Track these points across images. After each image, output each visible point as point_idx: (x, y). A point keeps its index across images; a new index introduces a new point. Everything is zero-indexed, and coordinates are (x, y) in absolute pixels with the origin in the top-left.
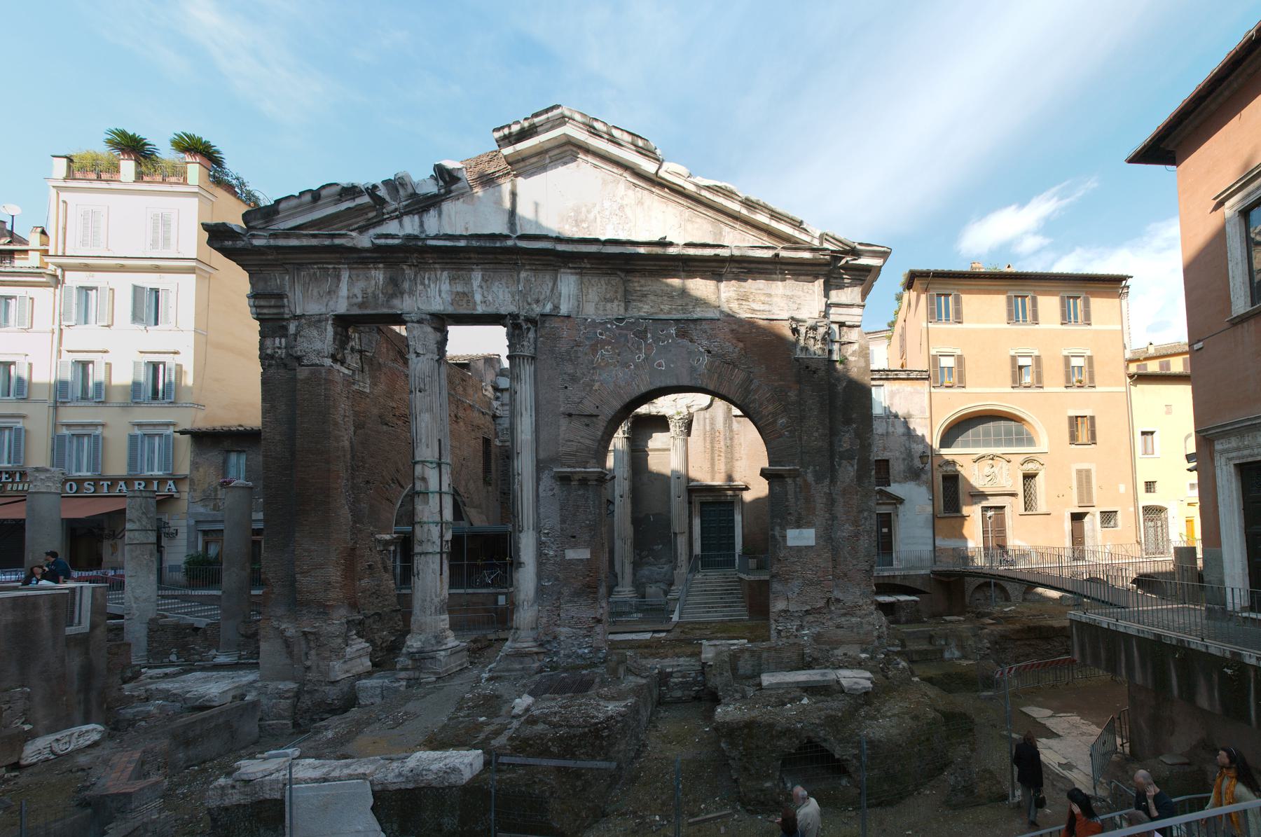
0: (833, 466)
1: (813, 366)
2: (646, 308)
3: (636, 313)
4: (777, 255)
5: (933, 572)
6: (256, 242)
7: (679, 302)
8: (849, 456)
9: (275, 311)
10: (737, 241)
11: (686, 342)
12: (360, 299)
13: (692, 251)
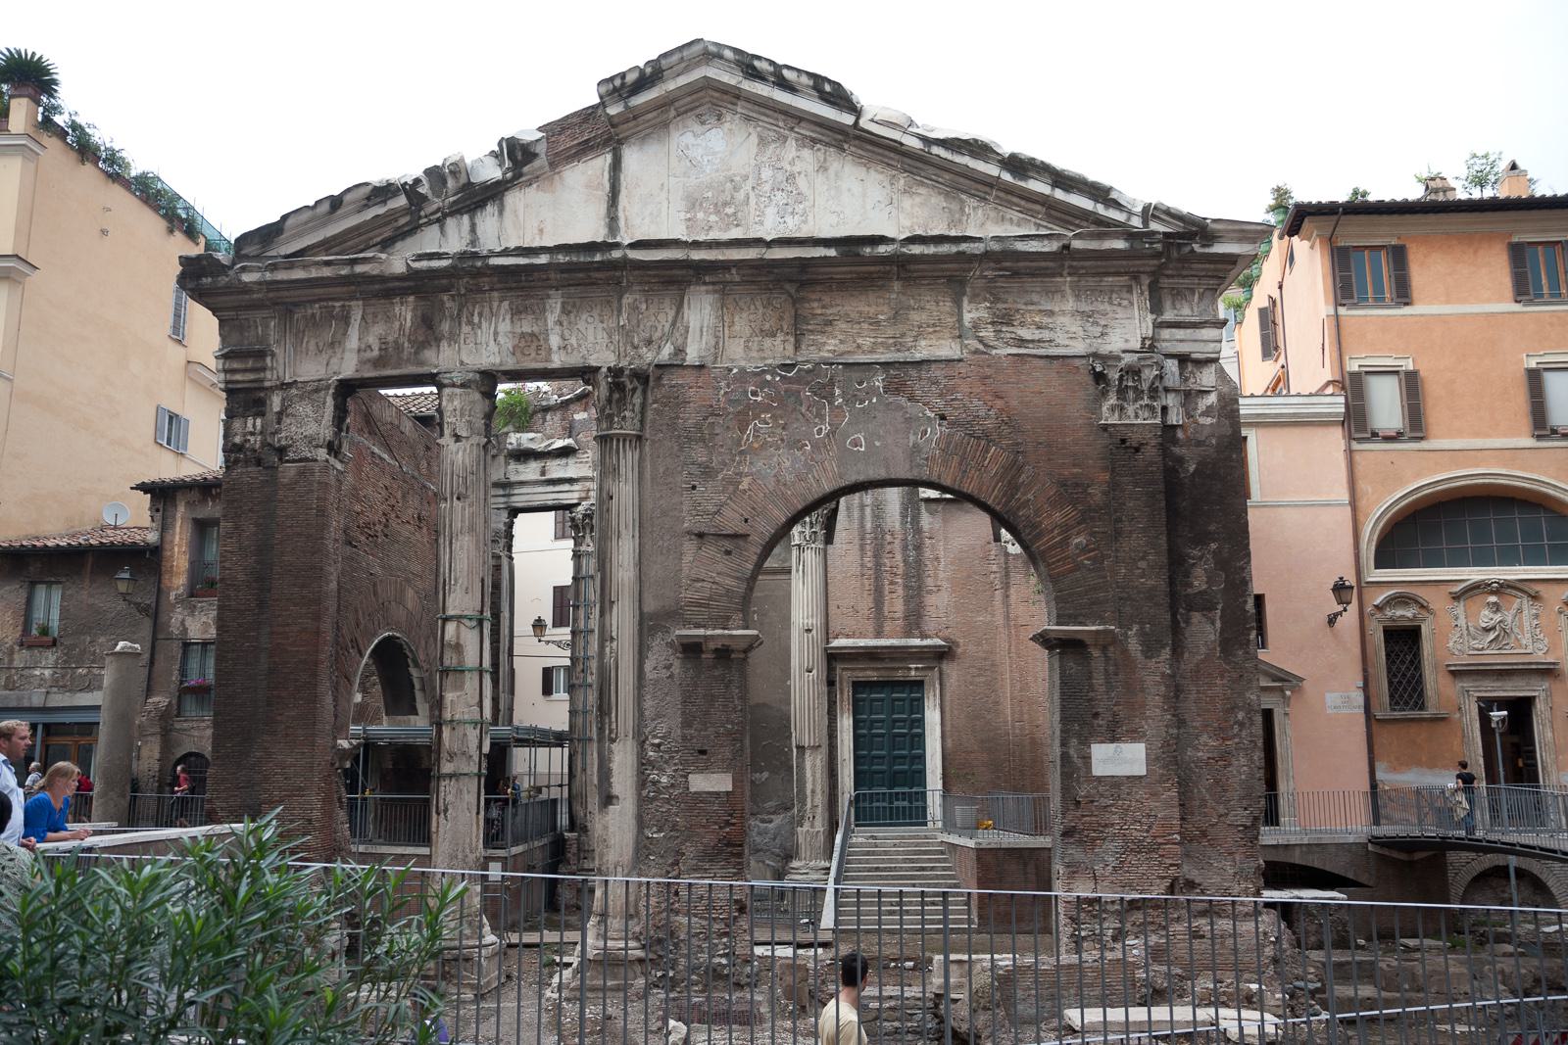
0: (1175, 623)
1: (1134, 438)
2: (832, 344)
3: (815, 355)
4: (1066, 247)
5: (1374, 840)
6: (247, 278)
7: (890, 332)
8: (1205, 604)
9: (251, 376)
10: (987, 225)
11: (903, 400)
12: (376, 353)
13: (916, 249)
